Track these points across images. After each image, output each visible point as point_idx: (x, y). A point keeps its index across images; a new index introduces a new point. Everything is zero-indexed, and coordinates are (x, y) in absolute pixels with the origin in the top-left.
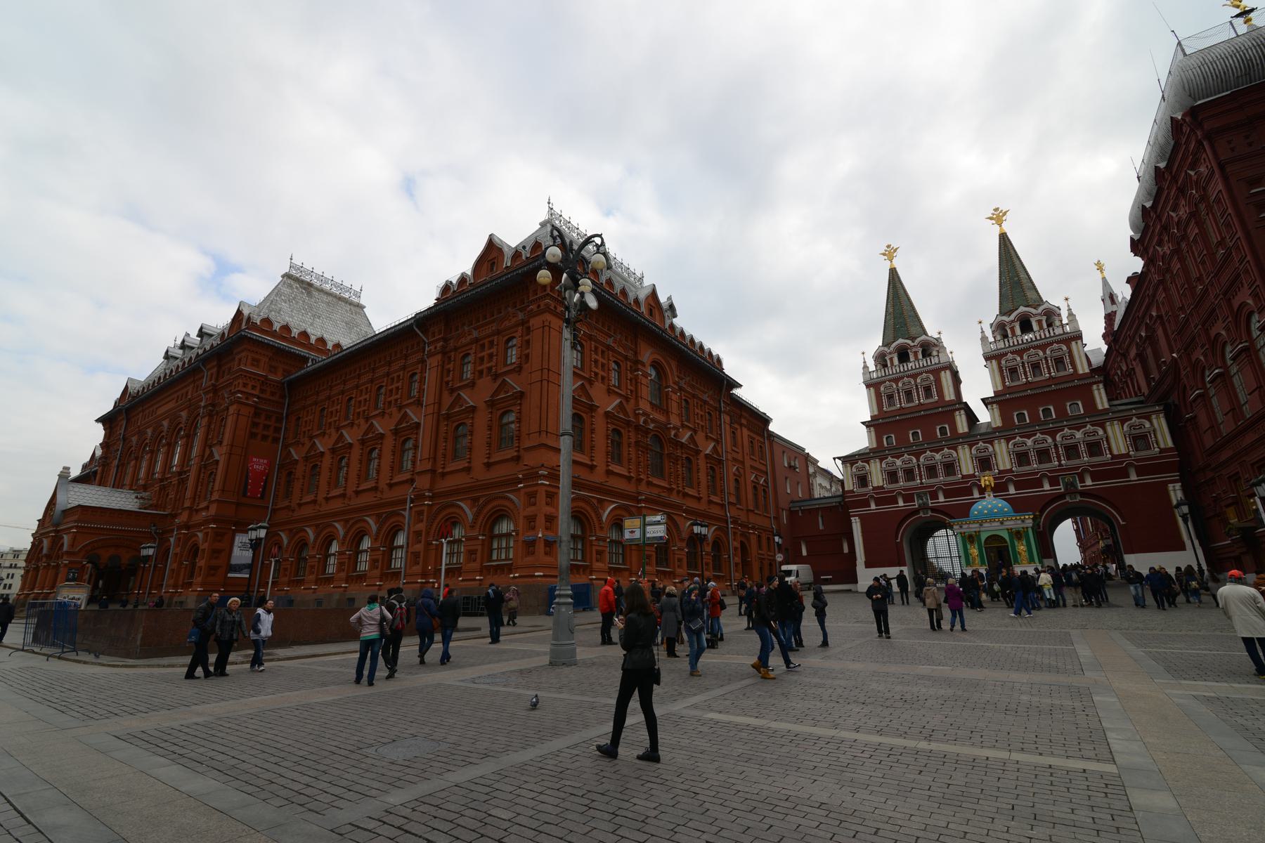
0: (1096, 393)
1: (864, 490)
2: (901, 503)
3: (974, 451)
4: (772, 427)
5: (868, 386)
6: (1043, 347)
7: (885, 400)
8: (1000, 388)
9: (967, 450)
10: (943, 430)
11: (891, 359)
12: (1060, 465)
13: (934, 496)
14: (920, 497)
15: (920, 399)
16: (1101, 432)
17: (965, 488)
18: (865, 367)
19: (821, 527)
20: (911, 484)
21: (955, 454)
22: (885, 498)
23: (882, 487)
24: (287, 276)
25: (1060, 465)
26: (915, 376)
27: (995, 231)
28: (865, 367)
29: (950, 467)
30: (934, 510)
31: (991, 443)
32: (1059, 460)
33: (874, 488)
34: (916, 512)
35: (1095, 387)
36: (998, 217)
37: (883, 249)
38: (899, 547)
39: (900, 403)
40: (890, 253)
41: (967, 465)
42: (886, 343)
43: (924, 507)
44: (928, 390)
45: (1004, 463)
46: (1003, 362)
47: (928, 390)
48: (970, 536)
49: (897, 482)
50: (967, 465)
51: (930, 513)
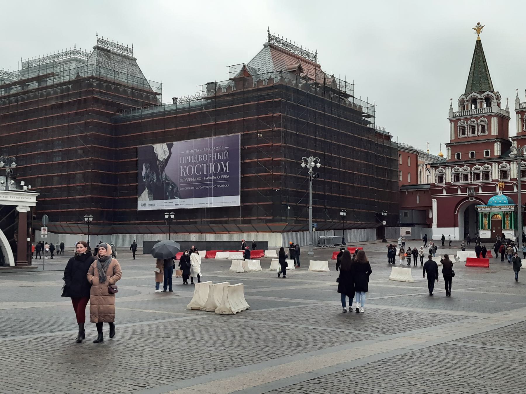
0: (496, 146)
1: (441, 184)
2: (459, 193)
3: (500, 167)
4: (392, 140)
5: (451, 121)
6: (477, 118)
7: (459, 131)
8: (520, 131)
9: (497, 166)
10: (487, 153)
11: (467, 104)
12: (471, 183)
13: (477, 190)
14: (469, 190)
15: (478, 132)
16: (490, 168)
17: (491, 188)
18: (451, 109)
19: (418, 202)
20: (466, 182)
21: (490, 168)
22: (452, 190)
23: (434, 184)
24: (97, 48)
25: (471, 183)
26: (477, 118)
27: (475, 38)
28: (451, 109)
29: (487, 175)
30: (476, 198)
31: (509, 163)
32: (471, 181)
33: (446, 184)
34: (467, 198)
35: (496, 144)
36: (478, 29)
37: (475, 25)
38: (456, 217)
39: (468, 133)
40: (478, 29)
41: (495, 175)
42: (466, 94)
43: (471, 196)
44: (483, 127)
45: (495, 176)
46: (459, 124)
47: (483, 127)
48: (485, 214)
49: (488, 179)
50: (495, 175)
51: (474, 199)
